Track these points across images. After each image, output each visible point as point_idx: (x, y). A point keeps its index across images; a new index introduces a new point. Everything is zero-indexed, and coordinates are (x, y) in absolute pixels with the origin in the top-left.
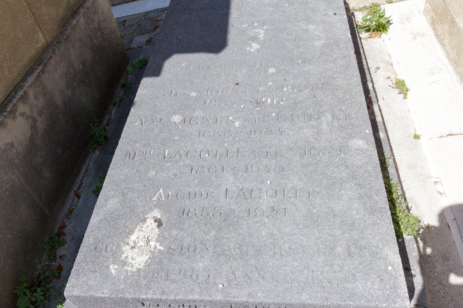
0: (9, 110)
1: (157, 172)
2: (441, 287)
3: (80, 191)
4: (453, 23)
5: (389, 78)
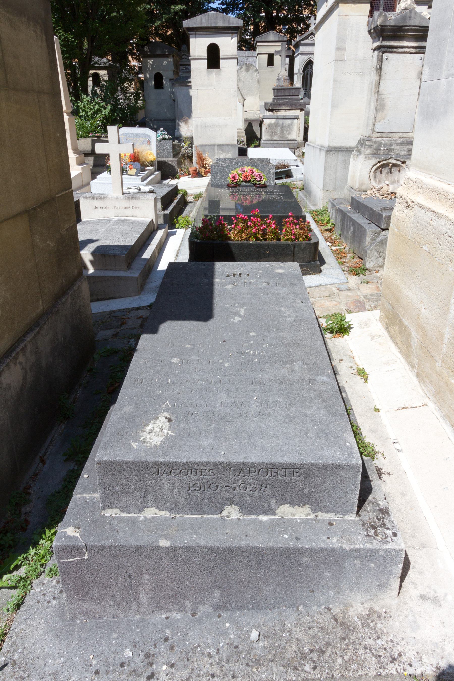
0: (13, 355)
1: (163, 391)
2: (400, 514)
3: (45, 457)
4: (401, 322)
5: (351, 367)
